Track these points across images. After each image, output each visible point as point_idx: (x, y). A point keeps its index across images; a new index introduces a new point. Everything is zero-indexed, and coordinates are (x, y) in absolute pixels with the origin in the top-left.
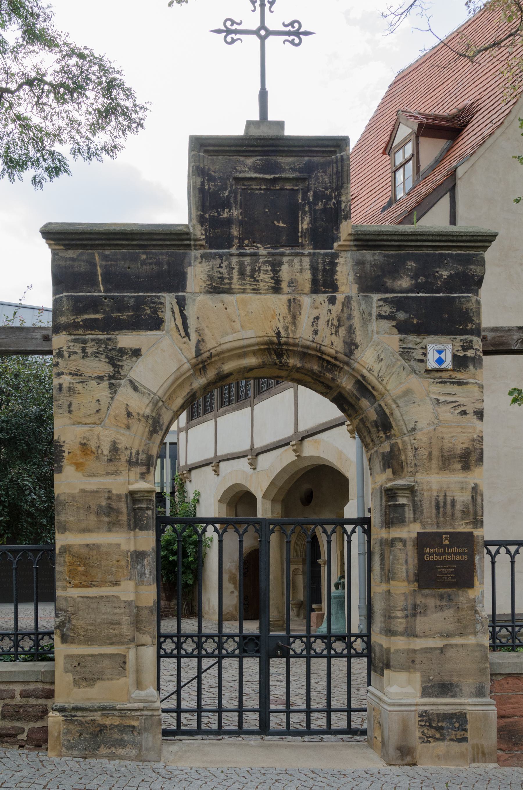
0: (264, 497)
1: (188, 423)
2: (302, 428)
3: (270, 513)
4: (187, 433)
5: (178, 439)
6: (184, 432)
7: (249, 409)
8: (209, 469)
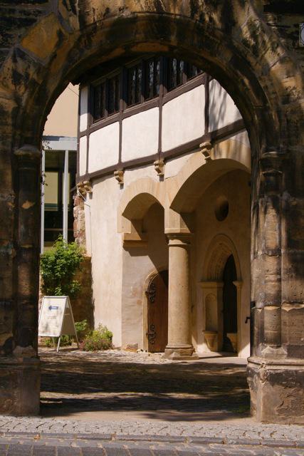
0: (172, 207)
1: (89, 126)
2: (164, 149)
3: (179, 226)
4: (88, 138)
5: (78, 146)
6: (86, 137)
7: (157, 108)
8: (112, 181)
